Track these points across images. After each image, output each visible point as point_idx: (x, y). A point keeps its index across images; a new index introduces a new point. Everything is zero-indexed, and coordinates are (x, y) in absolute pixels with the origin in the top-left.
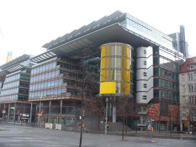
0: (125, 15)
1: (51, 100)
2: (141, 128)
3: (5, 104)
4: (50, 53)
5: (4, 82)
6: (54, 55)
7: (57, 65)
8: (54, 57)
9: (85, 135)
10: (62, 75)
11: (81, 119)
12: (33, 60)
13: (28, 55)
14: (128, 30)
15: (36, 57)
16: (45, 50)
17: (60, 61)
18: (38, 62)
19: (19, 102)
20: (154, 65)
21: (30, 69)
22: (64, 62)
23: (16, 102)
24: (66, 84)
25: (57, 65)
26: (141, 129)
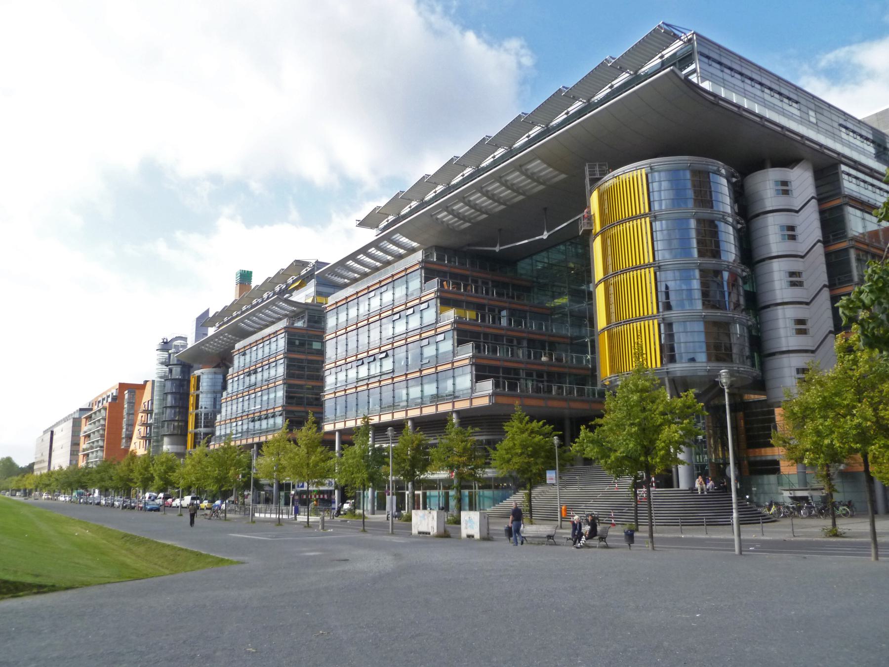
5: (230, 370)
7: (427, 279)
8: (413, 250)
10: (450, 315)
11: (314, 347)
17: (435, 267)
20: (826, 241)
24: (467, 351)
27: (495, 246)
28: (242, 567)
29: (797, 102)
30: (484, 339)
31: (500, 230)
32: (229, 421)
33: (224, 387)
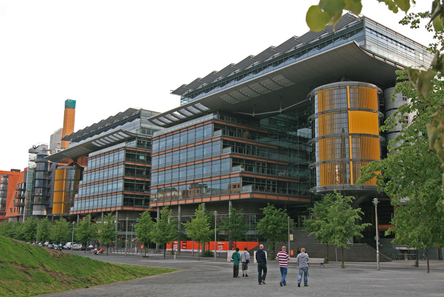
0: (362, 20)
1: (182, 205)
2: (406, 254)
3: (79, 214)
4: (196, 105)
6: (205, 108)
7: (216, 129)
9: (430, 261)
12: (155, 121)
13: (136, 110)
14: (374, 54)
15: (164, 115)
16: (176, 102)
18: (168, 126)
19: (126, 208)
21: (150, 140)
22: (229, 124)
23: (119, 209)
25: (216, 129)
26: (406, 257)
27: (252, 113)
28: (131, 266)
29: (413, 50)
30: (246, 163)
31: (255, 105)
32: (84, 198)
33: (81, 179)
